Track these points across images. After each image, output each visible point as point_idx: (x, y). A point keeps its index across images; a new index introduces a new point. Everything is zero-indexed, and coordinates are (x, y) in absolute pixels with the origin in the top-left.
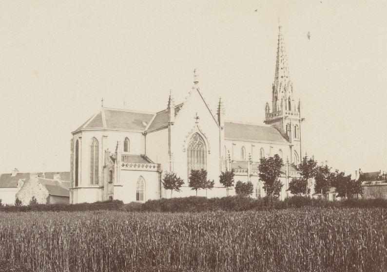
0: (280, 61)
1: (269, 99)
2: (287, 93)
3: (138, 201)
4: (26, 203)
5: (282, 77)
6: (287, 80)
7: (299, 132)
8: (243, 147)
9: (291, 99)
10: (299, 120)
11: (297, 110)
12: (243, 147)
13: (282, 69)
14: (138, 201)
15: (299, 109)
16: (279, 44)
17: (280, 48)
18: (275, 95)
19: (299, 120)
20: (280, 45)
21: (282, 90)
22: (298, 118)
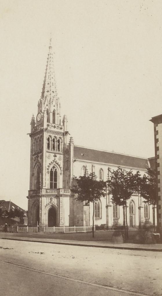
0: (47, 77)
1: (35, 111)
2: (52, 106)
3: (85, 164)
4: (57, 162)
5: (48, 91)
6: (53, 94)
7: (134, 220)
8: (101, 169)
9: (56, 113)
10: (63, 134)
11: (62, 124)
12: (101, 169)
13: (48, 84)
14: (85, 164)
15: (64, 122)
16: (46, 70)
17: (48, 66)
18: (107, 210)
19: (63, 134)
20: (48, 71)
21: (46, 103)
22: (62, 131)
